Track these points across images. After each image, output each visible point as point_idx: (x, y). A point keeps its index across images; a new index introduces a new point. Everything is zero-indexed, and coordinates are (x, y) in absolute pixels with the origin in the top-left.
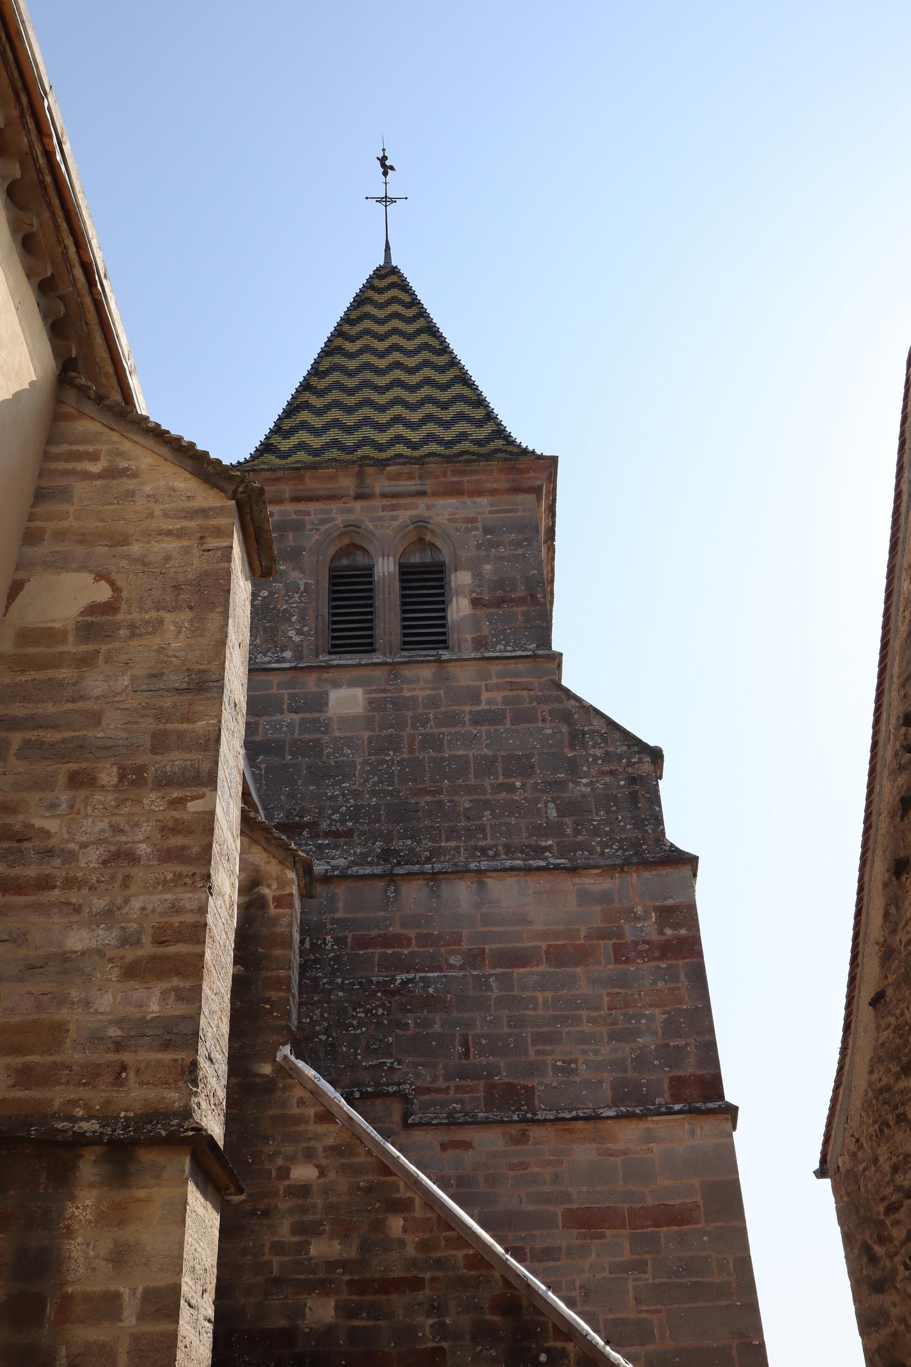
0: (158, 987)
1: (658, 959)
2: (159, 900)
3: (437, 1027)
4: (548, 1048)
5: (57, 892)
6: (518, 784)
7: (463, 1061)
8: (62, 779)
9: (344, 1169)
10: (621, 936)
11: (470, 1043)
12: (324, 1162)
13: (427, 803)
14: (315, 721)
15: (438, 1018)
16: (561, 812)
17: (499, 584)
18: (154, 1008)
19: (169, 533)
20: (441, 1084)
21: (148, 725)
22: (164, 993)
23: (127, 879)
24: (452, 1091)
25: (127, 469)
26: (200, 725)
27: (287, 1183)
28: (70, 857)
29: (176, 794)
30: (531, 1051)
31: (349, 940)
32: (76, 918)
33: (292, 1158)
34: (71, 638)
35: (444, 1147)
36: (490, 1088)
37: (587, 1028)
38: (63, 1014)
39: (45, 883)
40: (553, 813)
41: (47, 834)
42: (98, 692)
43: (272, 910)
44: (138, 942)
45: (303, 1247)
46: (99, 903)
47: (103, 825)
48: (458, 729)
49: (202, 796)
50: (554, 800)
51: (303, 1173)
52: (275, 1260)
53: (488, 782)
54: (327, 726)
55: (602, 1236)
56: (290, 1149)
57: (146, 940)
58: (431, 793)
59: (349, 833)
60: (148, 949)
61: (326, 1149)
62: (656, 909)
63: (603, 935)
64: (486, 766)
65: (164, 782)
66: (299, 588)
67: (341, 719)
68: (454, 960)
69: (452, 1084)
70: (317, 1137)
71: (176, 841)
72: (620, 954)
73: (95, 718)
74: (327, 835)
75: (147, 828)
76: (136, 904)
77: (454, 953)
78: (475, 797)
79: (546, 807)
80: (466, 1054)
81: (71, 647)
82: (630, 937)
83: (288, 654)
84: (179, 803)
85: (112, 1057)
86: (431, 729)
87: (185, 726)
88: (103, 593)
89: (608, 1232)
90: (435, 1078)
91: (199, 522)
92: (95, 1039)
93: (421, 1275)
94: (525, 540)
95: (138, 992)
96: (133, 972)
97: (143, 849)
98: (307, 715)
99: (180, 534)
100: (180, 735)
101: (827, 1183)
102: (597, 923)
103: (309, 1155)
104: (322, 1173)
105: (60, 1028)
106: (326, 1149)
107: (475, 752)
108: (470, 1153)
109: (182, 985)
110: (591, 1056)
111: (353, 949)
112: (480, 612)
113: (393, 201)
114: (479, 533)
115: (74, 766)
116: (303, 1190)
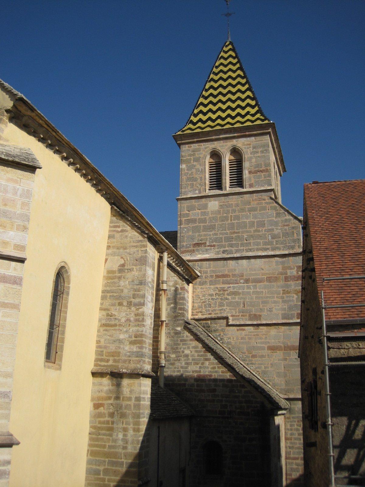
0: (136, 346)
1: (296, 280)
2: (135, 329)
3: (237, 300)
4: (265, 305)
5: (117, 327)
6: (261, 230)
7: (243, 308)
8: (117, 304)
9: (196, 351)
10: (287, 274)
11: (245, 304)
12: (191, 350)
13: (235, 236)
14: (205, 212)
15: (237, 297)
16: (273, 238)
17: (258, 166)
18: (135, 350)
19: (134, 246)
20: (237, 314)
21: (132, 292)
22: (137, 347)
23: (129, 325)
24: (240, 316)
25: (125, 230)
26: (141, 293)
27: (184, 354)
28: (119, 320)
29: (137, 307)
30: (261, 306)
31: (214, 276)
32: (121, 332)
33: (184, 349)
34: (117, 272)
35: (238, 330)
36: (250, 315)
37: (276, 299)
38: (120, 350)
39: (115, 325)
40: (270, 238)
41: (115, 315)
42: (123, 285)
43: (180, 291)
44: (131, 337)
45: (187, 368)
46: (125, 329)
47: (124, 314)
48: (244, 213)
49: (142, 308)
50: (270, 234)
51: (187, 352)
52: (182, 370)
53: (252, 230)
54: (208, 214)
55: (277, 352)
56: (184, 346)
57: (133, 337)
58: (236, 233)
59: (214, 246)
60: (134, 339)
61: (192, 347)
62: (297, 266)
63: (281, 274)
64: (252, 224)
65: (135, 305)
66: (200, 170)
67: (212, 211)
68: (242, 281)
69: (240, 314)
70: (190, 344)
71: (137, 317)
72: (286, 279)
73: (122, 291)
74: (208, 246)
75: (133, 314)
76: (131, 330)
77: (241, 279)
78: (249, 234)
79: (268, 236)
80: (244, 306)
81: (118, 275)
82: (289, 274)
83: (197, 192)
84: (138, 309)
85: (128, 358)
86: (237, 213)
87: (139, 293)
88: (122, 262)
89: (278, 352)
90: (236, 312)
91: (140, 243)
92: (126, 355)
93: (212, 374)
94: (265, 150)
95: (132, 347)
96: (132, 343)
97: (132, 319)
98: (203, 210)
99: (136, 247)
100: (138, 295)
101: (299, 358)
102: (280, 270)
103: (189, 348)
104: (191, 352)
105: (119, 353)
106: (192, 347)
107: (249, 220)
108: (245, 331)
109: (139, 345)
110: (277, 307)
111: (215, 278)
112: (252, 175)
113: (230, 15)
114: (251, 149)
115: (119, 301)
116: (187, 356)
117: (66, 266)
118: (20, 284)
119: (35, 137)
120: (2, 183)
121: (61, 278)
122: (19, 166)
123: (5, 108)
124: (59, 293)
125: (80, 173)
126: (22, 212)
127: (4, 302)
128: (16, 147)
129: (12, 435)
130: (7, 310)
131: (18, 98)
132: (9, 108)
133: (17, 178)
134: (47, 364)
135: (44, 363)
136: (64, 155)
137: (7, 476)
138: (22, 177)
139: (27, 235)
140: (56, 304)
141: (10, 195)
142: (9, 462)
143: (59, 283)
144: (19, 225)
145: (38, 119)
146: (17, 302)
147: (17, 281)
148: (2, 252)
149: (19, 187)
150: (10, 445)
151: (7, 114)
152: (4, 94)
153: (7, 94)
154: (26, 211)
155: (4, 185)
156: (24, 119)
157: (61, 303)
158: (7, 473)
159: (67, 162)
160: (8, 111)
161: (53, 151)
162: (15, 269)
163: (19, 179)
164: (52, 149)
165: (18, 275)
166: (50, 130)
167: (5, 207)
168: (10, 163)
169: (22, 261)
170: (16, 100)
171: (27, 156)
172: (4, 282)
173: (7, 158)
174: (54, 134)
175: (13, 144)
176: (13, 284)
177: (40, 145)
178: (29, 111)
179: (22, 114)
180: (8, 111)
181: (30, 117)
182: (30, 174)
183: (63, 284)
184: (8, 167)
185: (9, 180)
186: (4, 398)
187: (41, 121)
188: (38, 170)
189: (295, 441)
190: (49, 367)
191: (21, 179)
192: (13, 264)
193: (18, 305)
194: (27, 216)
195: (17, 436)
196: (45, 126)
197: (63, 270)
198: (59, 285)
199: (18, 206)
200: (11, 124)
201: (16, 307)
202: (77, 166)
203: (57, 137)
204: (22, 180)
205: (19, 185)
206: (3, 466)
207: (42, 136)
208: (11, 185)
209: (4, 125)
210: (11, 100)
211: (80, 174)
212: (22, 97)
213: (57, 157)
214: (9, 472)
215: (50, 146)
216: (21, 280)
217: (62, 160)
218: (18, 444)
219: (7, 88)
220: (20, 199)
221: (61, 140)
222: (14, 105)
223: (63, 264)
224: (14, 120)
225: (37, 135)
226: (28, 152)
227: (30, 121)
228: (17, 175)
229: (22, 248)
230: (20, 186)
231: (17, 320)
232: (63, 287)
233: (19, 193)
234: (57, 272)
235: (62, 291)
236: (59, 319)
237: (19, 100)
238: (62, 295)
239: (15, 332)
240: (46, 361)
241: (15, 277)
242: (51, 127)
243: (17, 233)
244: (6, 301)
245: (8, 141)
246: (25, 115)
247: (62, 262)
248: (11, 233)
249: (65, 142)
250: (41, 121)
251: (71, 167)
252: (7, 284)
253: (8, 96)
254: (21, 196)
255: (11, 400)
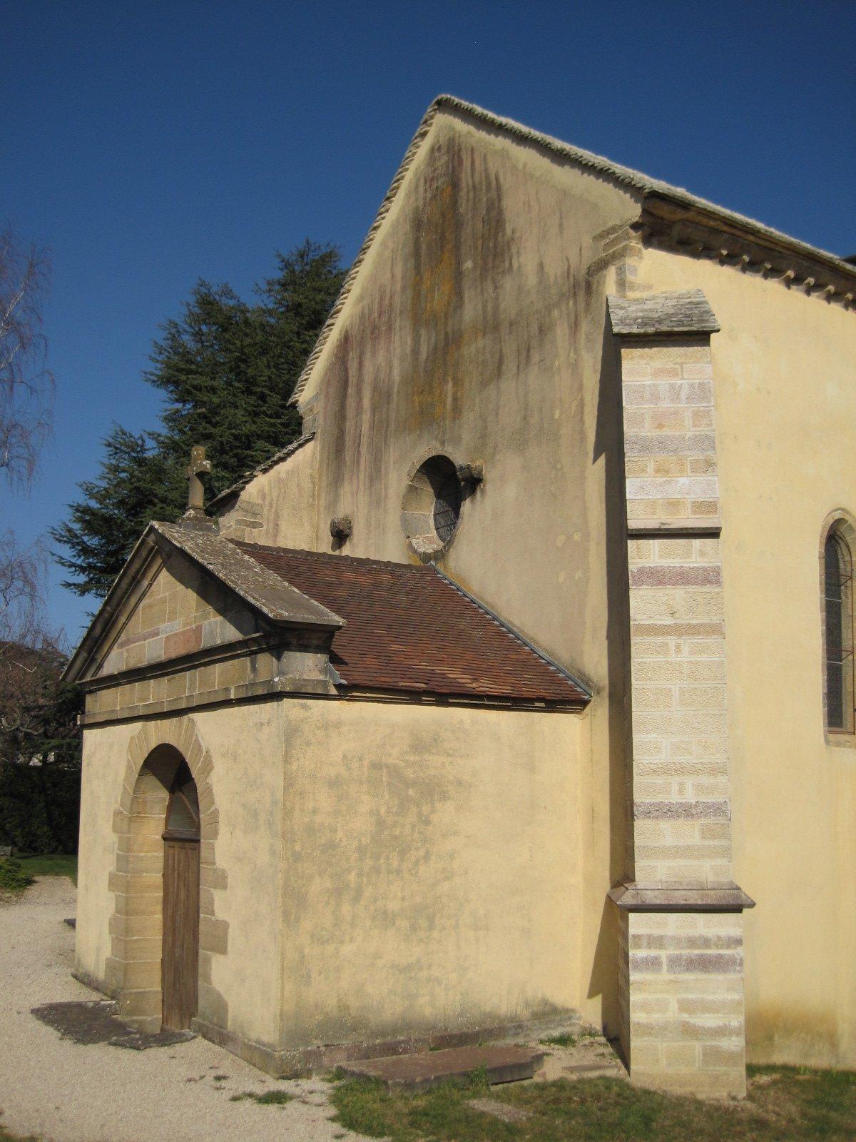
117: (847, 517)
118: (718, 582)
119: (710, 257)
120: (646, 383)
121: (843, 545)
122: (673, 338)
123: (628, 223)
124: (843, 580)
125: (840, 302)
126: (698, 433)
127: (689, 625)
128: (668, 295)
129: (738, 889)
130: (698, 640)
131: (646, 195)
132: (636, 219)
133: (674, 364)
134: (831, 737)
135: (826, 737)
136: (789, 276)
137: (738, 968)
138: (683, 360)
139: (716, 478)
140: (840, 604)
141: (665, 405)
142: (738, 942)
143: (840, 557)
144: (697, 461)
145: (705, 220)
146: (716, 619)
147: (710, 577)
148: (669, 524)
149: (682, 381)
150: (737, 909)
151: (636, 232)
152: (621, 192)
153: (625, 192)
154: (706, 429)
155: (649, 386)
156: (676, 231)
157: (850, 600)
158: (738, 961)
159: (802, 287)
160: (635, 226)
161: (762, 273)
162: (702, 553)
163: (678, 366)
164: (757, 271)
165: (711, 565)
166: (739, 233)
167: (659, 430)
168: (653, 338)
169: (713, 533)
170: (646, 198)
171: (691, 309)
172: (683, 584)
173: (642, 331)
174: (752, 238)
175: (664, 290)
176: (704, 584)
177: (727, 271)
178: (679, 210)
179: (668, 223)
180: (635, 226)
181: (685, 222)
182: (699, 348)
183: (847, 558)
184: (651, 347)
185: (657, 373)
186: (715, 815)
187: (712, 223)
188: (713, 336)
189: (652, 953)
190: (838, 744)
191: (681, 364)
192: (697, 543)
193: (720, 626)
194: (708, 437)
195: (749, 891)
196: (726, 228)
197: (843, 528)
198: (841, 561)
199: (686, 423)
200: (650, 250)
201: (715, 630)
202: (827, 289)
203: (760, 242)
204: (685, 366)
205: (680, 377)
206: (727, 948)
207: (725, 252)
208: (664, 383)
209: (636, 258)
210: (636, 201)
211: (843, 303)
212: (652, 189)
213: (774, 285)
214: (741, 960)
215: (752, 266)
216: (719, 574)
217: (789, 287)
218: (752, 905)
219: (623, 180)
220: (688, 408)
221: (772, 246)
222: (645, 212)
223: (838, 515)
224: (655, 240)
225: (713, 254)
226: (693, 300)
227: (689, 230)
228: (671, 359)
229: (711, 507)
230: (683, 379)
231: (723, 656)
232: (849, 565)
233: (683, 396)
234: (825, 534)
235: (849, 574)
236: (850, 637)
237: (651, 197)
238: (849, 583)
239: (721, 682)
240: (830, 732)
241: (705, 569)
242: (740, 227)
243: (694, 478)
244: (694, 622)
245: (649, 287)
246: (674, 222)
247: (839, 509)
248: (683, 481)
249: (783, 247)
250: (712, 223)
251: (814, 295)
252: (691, 586)
253: (628, 195)
254: (689, 399)
255: (730, 820)
